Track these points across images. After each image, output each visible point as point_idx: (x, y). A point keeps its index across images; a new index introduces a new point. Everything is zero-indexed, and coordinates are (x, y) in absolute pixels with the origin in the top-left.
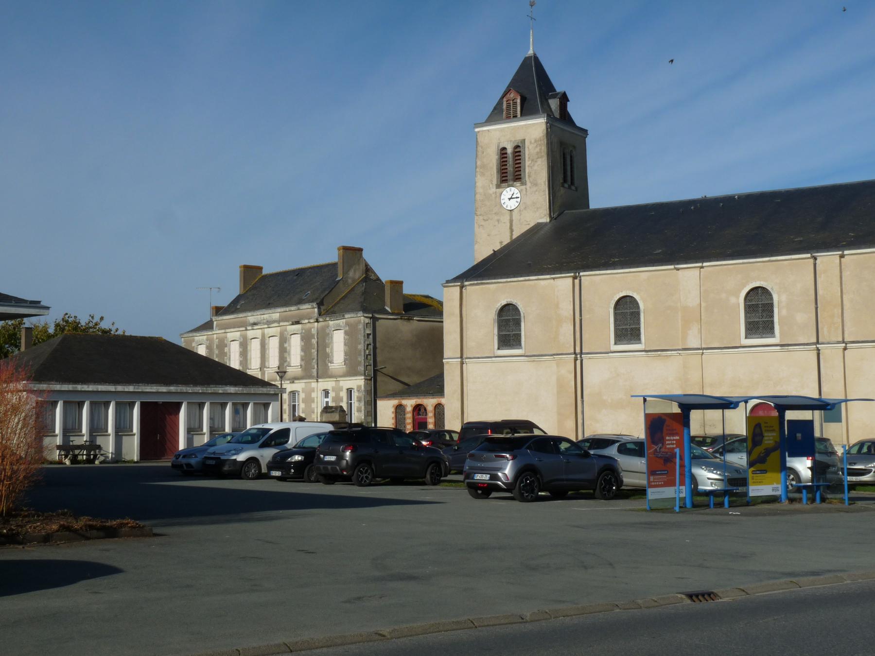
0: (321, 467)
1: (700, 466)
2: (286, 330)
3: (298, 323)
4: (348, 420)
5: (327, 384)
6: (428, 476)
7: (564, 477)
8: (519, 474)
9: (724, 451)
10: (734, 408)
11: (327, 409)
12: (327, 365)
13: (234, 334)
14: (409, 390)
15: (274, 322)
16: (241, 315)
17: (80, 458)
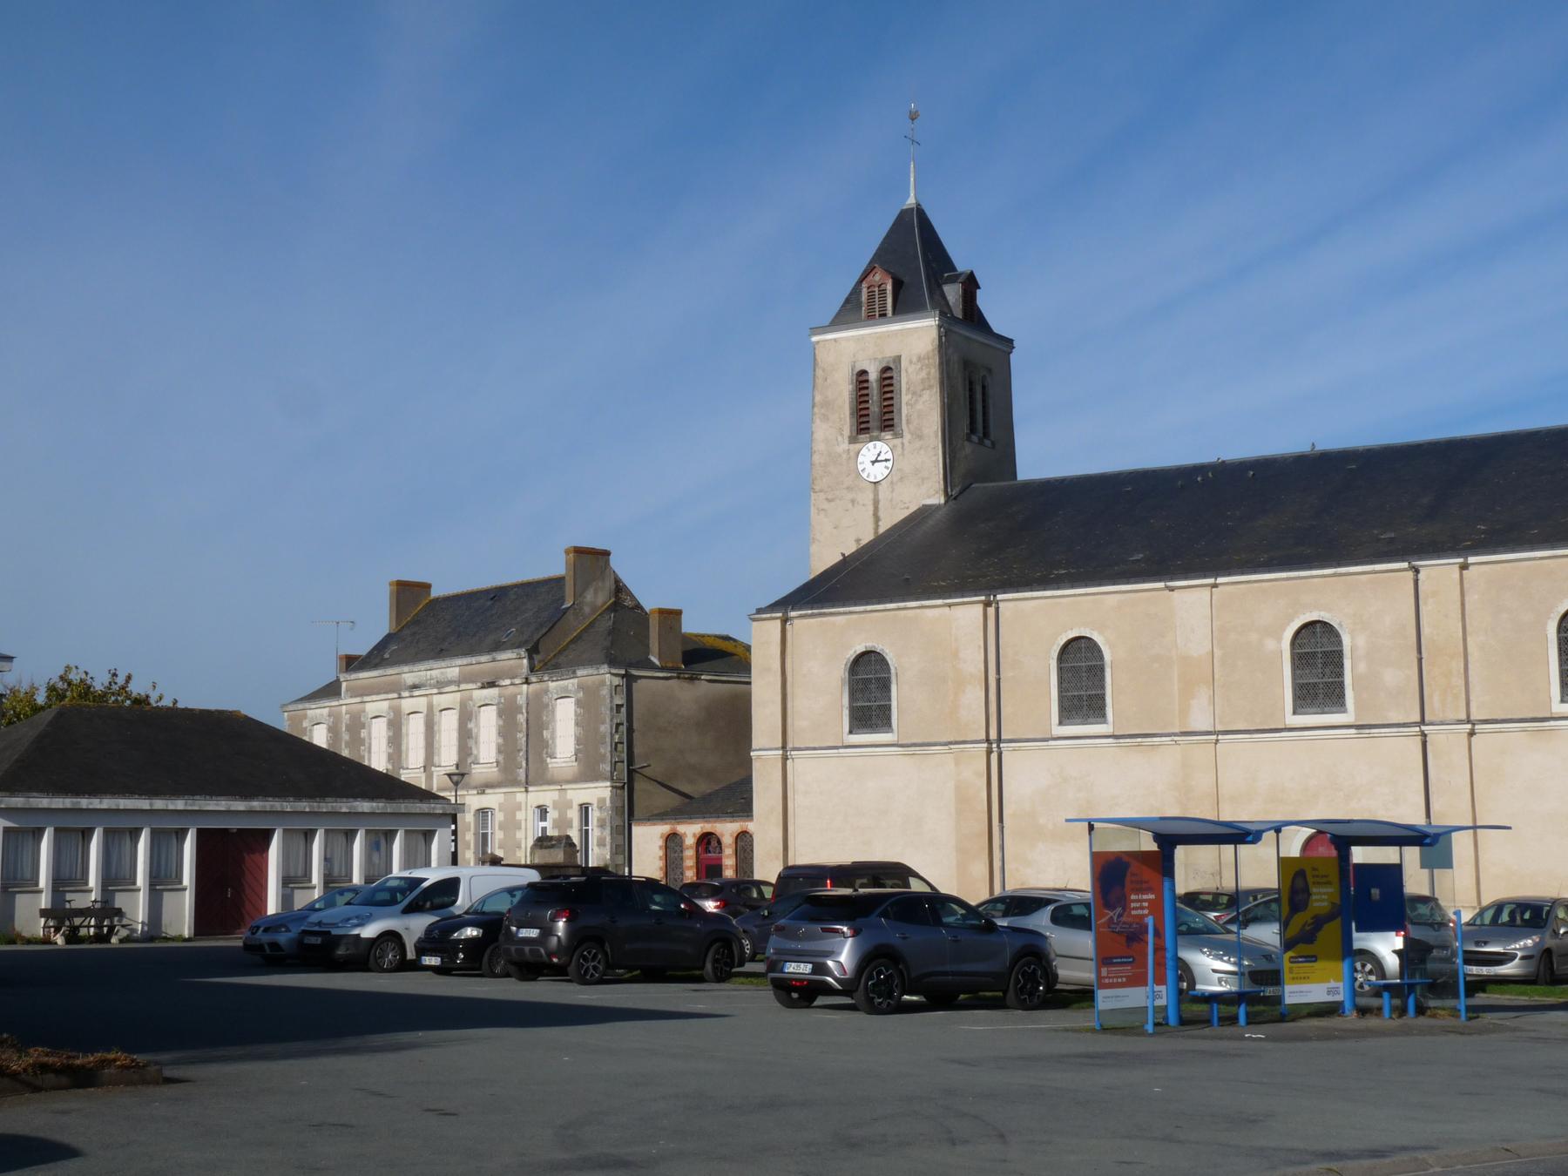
0: (513, 948)
1: (1199, 947)
2: (471, 699)
3: (492, 685)
4: (580, 860)
5: (544, 795)
6: (709, 966)
7: (948, 968)
8: (865, 962)
9: (1247, 920)
10: (1253, 842)
11: (543, 842)
12: (543, 762)
13: (377, 706)
14: (690, 807)
15: (450, 683)
16: (390, 671)
17: (83, 932)
